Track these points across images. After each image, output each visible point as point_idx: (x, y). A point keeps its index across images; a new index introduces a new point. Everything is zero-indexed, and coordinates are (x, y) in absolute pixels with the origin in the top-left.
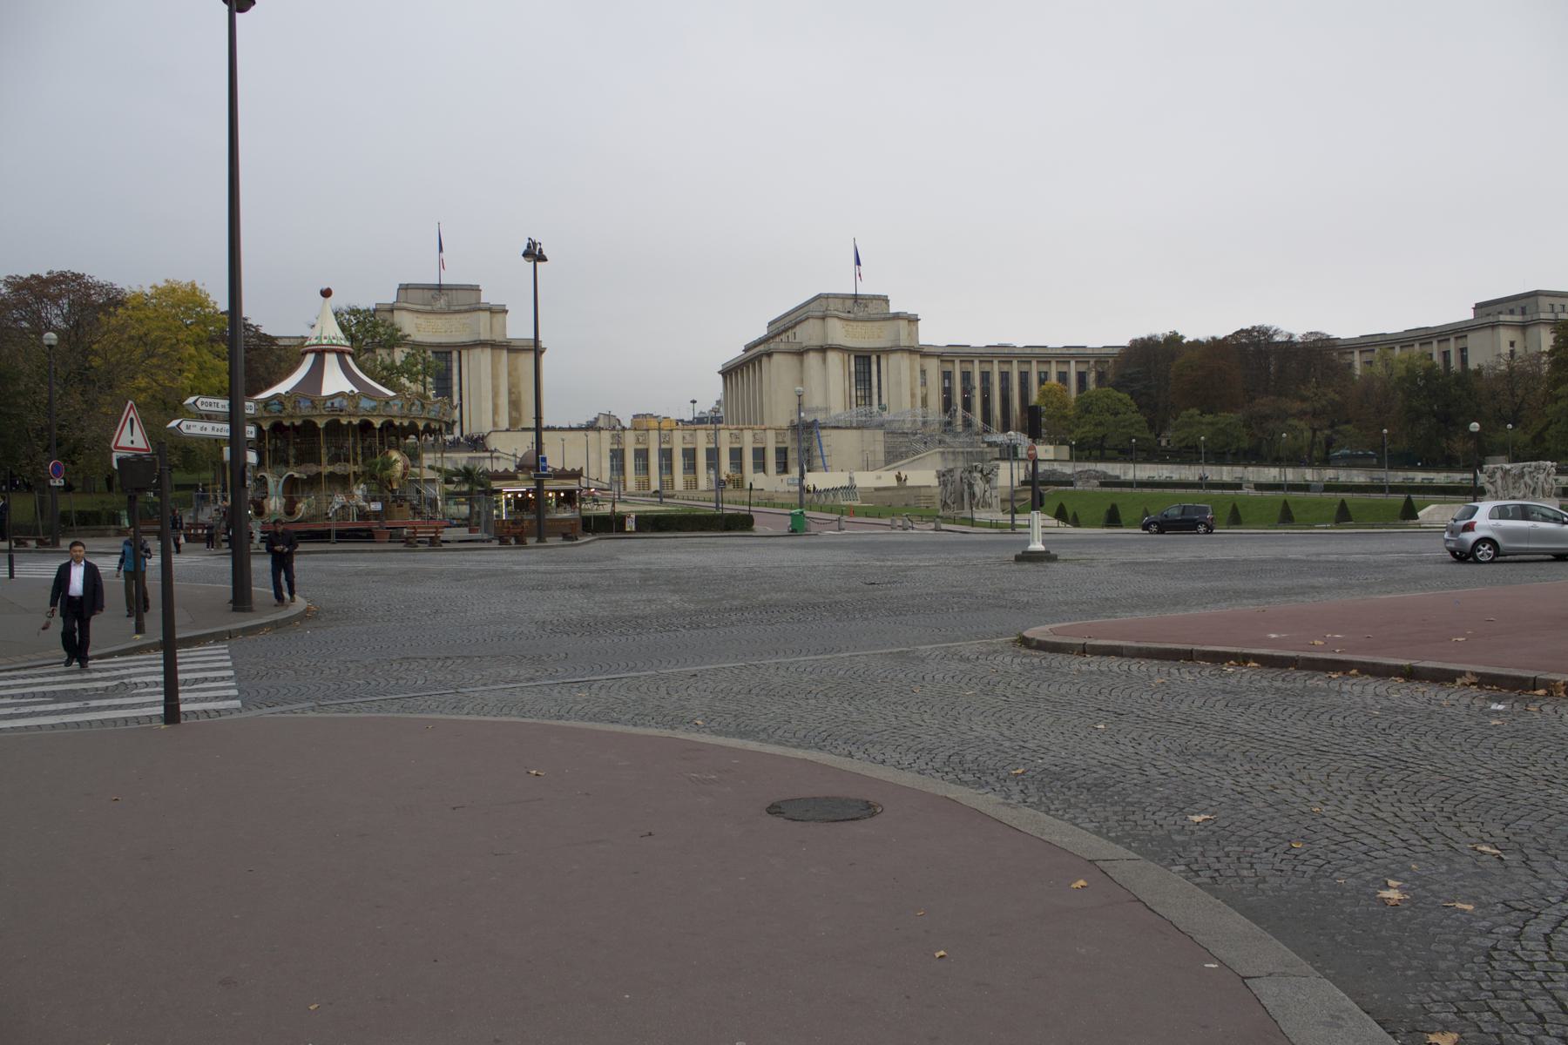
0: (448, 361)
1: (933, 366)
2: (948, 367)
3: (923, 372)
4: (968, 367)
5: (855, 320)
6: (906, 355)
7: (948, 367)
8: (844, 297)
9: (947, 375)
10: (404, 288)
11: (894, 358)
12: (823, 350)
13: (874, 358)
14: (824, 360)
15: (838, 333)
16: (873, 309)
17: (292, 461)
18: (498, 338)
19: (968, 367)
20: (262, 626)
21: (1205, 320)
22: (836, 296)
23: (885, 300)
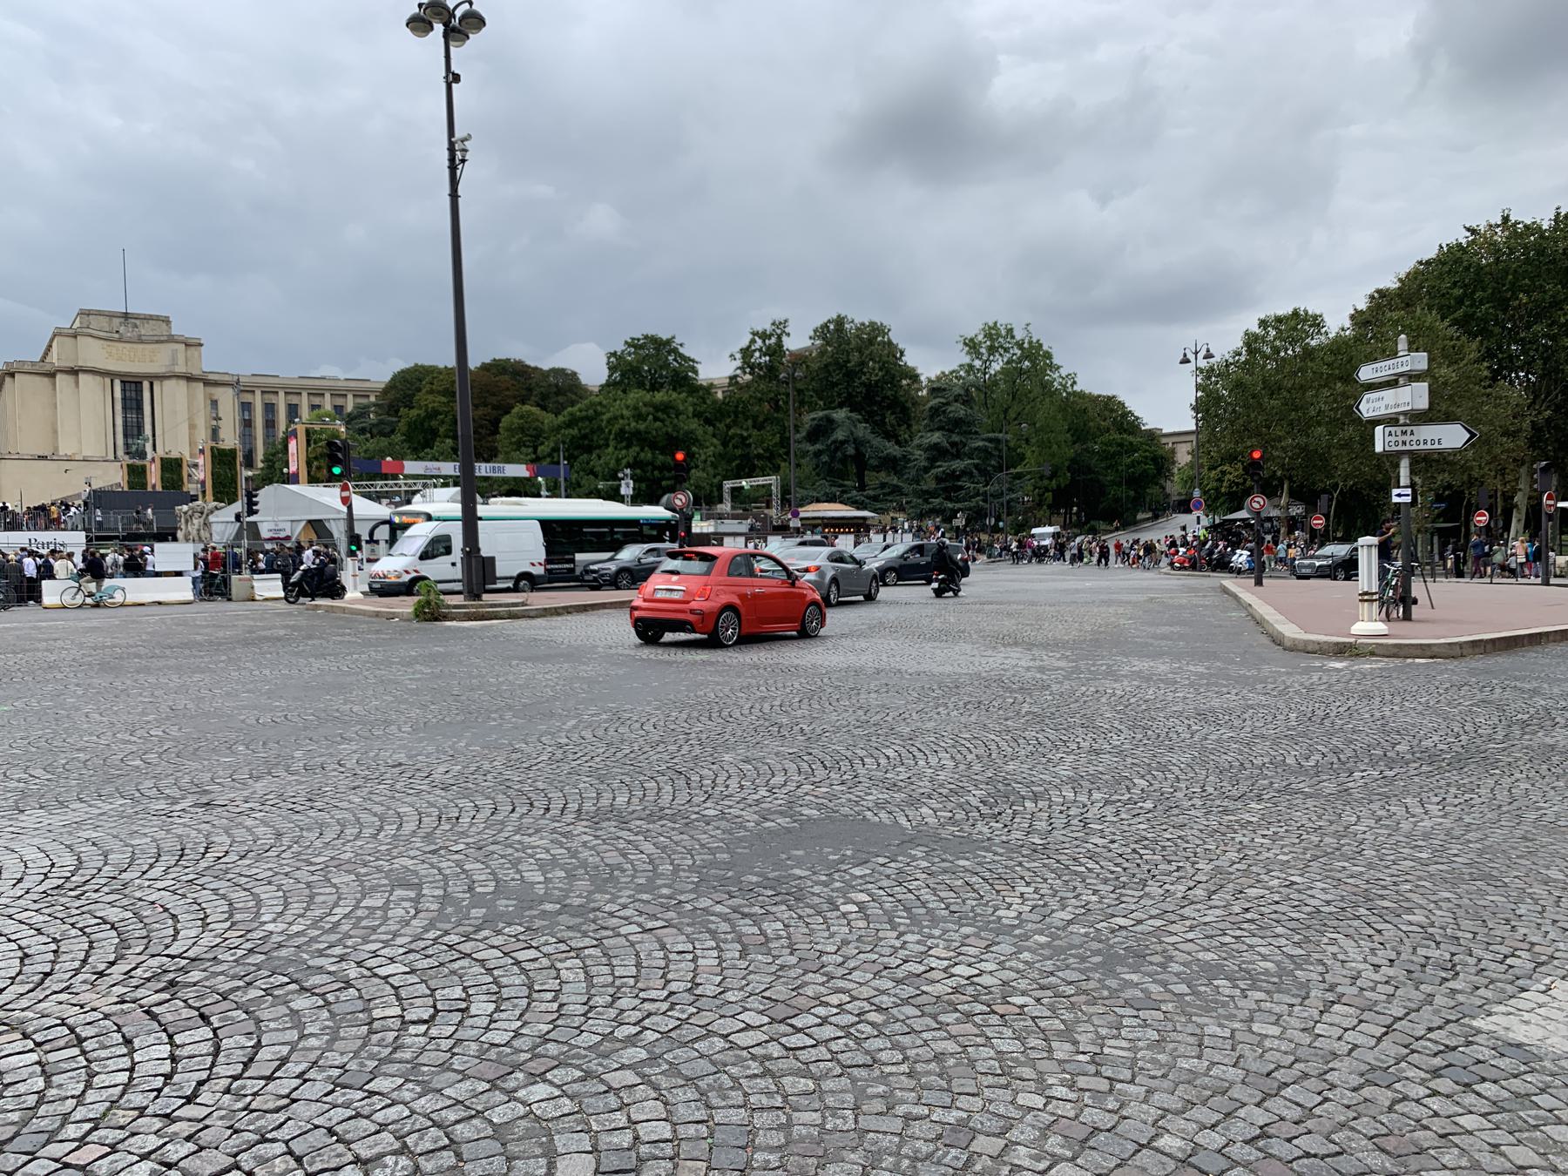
0: (140, 392)
1: (226, 397)
2: (247, 398)
3: (214, 403)
4: (271, 399)
5: (120, 340)
6: (183, 383)
7: (247, 398)
8: (111, 315)
9: (246, 407)
10: (85, 313)
11: (167, 383)
12: (74, 372)
13: (146, 385)
14: (77, 383)
15: (94, 353)
16: (146, 330)
17: (544, 493)
18: (196, 372)
19: (271, 399)
20: (603, 606)
21: (427, 363)
22: (100, 313)
23: (167, 321)
